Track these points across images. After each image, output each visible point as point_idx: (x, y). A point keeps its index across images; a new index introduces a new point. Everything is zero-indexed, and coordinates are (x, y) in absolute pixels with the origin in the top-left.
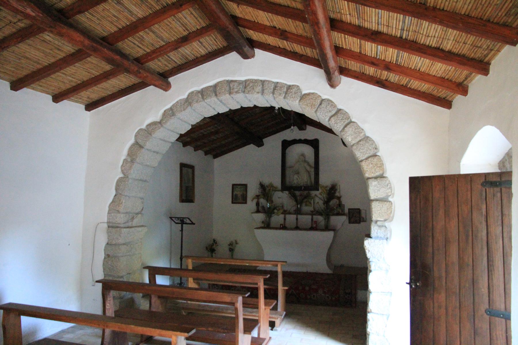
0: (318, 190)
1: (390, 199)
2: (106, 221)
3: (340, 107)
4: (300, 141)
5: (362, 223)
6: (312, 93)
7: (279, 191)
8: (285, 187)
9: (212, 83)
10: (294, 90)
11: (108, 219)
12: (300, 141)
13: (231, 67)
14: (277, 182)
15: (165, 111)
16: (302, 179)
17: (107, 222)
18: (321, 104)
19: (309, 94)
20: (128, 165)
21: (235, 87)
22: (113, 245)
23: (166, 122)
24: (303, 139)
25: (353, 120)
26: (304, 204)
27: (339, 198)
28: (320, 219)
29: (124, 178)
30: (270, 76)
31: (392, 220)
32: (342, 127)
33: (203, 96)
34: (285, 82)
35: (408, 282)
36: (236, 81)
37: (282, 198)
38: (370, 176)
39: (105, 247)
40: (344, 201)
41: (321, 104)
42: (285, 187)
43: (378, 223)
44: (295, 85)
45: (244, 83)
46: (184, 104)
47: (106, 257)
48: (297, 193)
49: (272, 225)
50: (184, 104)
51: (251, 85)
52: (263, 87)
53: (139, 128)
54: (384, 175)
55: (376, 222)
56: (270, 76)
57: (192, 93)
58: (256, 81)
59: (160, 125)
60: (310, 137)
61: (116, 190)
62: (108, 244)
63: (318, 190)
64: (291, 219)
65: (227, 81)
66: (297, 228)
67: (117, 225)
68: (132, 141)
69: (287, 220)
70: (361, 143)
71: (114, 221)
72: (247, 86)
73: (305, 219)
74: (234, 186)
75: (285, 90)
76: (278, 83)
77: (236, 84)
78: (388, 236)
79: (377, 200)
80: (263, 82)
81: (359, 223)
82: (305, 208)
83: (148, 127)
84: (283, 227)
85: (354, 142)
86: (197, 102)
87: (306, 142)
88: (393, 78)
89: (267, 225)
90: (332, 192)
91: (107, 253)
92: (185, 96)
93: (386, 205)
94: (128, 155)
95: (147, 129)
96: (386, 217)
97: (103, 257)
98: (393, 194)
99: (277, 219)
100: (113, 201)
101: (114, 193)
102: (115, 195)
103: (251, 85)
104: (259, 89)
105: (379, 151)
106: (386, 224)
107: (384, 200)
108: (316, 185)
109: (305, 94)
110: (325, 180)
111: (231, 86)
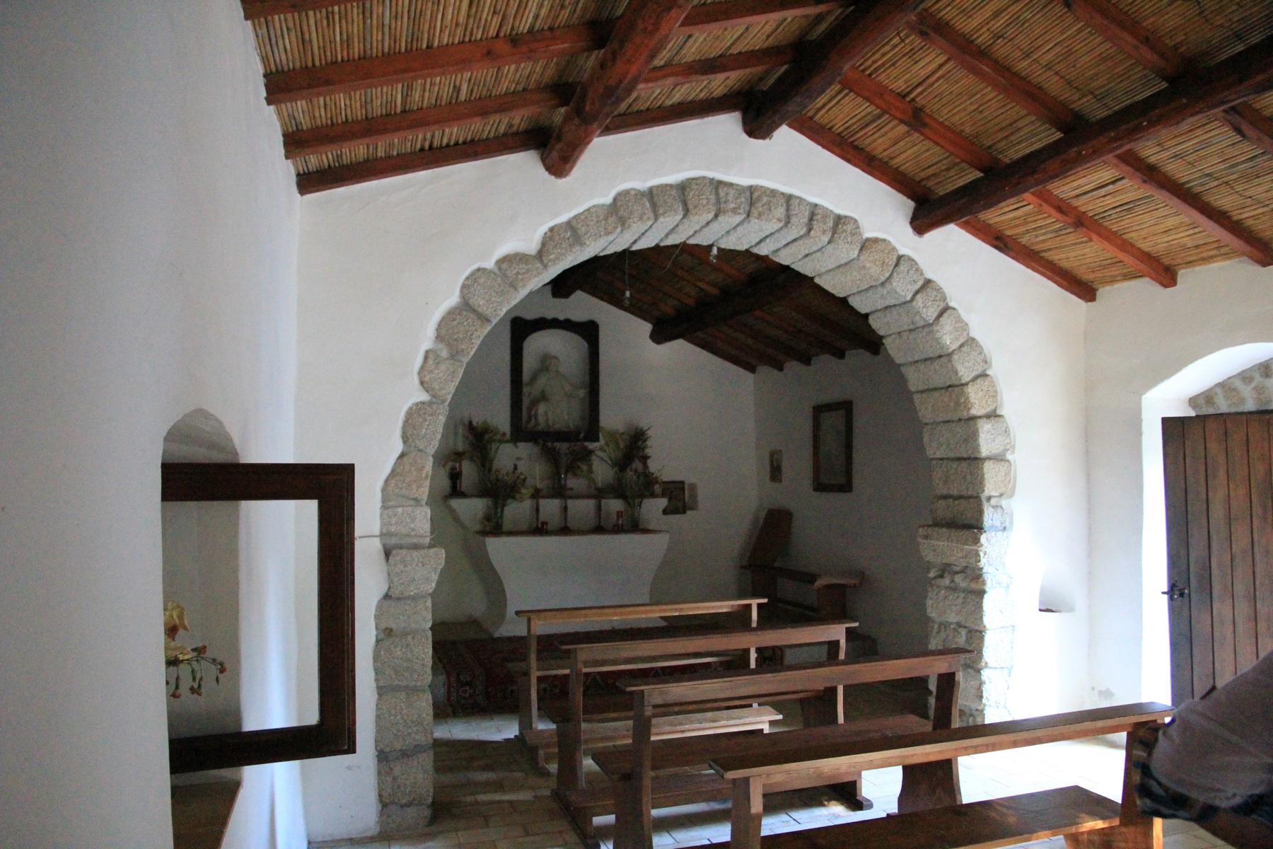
0: (597, 440)
1: (1009, 456)
2: (377, 532)
3: (929, 275)
4: (555, 324)
5: (689, 512)
6: (884, 240)
7: (506, 442)
8: (521, 431)
9: (674, 178)
10: (849, 227)
11: (383, 524)
12: (555, 324)
13: (712, 149)
14: (500, 418)
15: (551, 230)
16: (559, 411)
17: (382, 535)
18: (897, 265)
19: (876, 240)
20: (443, 367)
21: (730, 198)
22: (409, 597)
23: (557, 258)
24: (562, 318)
25: (952, 304)
26: (569, 475)
27: (645, 459)
28: (614, 505)
29: (430, 403)
30: (799, 190)
31: (1012, 496)
32: (935, 315)
33: (654, 206)
34: (831, 207)
35: (1166, 590)
36: (731, 185)
37: (513, 458)
38: (979, 414)
39: (379, 607)
40: (653, 466)
41: (897, 265)
42: (521, 431)
43: (993, 501)
44: (852, 218)
45: (748, 194)
46: (606, 219)
47: (382, 636)
48: (563, 447)
49: (507, 525)
50: (606, 219)
51: (765, 199)
52: (788, 210)
53: (475, 266)
54: (998, 412)
55: (989, 498)
56: (799, 190)
57: (626, 193)
58: (773, 193)
59: (539, 265)
60: (579, 316)
61: (405, 438)
62: (387, 597)
63: (597, 440)
64: (550, 507)
65: (712, 180)
66: (565, 530)
67: (415, 541)
68: (453, 300)
69: (571, 512)
70: (965, 349)
71: (404, 531)
72: (754, 199)
73: (582, 508)
74: (841, 480)
75: (831, 224)
76: (816, 205)
77: (732, 192)
78: (1007, 524)
79: (989, 458)
80: (789, 198)
81: (684, 512)
82: (573, 483)
83: (504, 266)
84: (540, 529)
85: (954, 347)
86: (641, 219)
87: (567, 325)
88: (357, 151)
89: (493, 526)
90: (634, 445)
91: (384, 625)
92: (608, 200)
93: (1002, 468)
94: (439, 338)
95: (500, 269)
96: (1003, 490)
97: (374, 639)
98: (1014, 447)
99: (518, 510)
100: (393, 473)
101: (399, 447)
102: (402, 456)
103: (765, 199)
104: (780, 212)
105: (990, 366)
106: (1004, 502)
107: (999, 458)
108: (591, 427)
109: (868, 240)
110: (612, 418)
111: (722, 194)
